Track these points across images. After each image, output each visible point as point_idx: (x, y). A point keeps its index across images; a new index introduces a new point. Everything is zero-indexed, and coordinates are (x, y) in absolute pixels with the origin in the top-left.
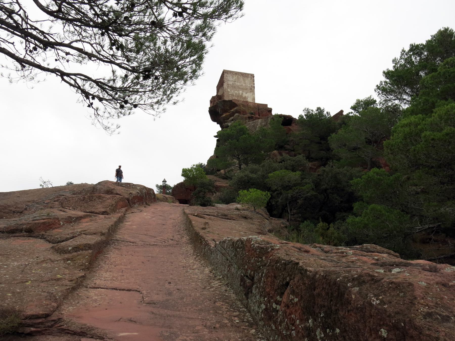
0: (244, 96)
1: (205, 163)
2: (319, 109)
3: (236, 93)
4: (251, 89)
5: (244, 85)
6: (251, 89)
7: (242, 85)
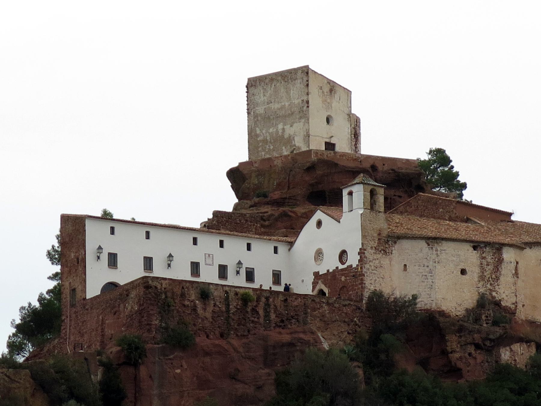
4: (301, 111)
7: (283, 107)
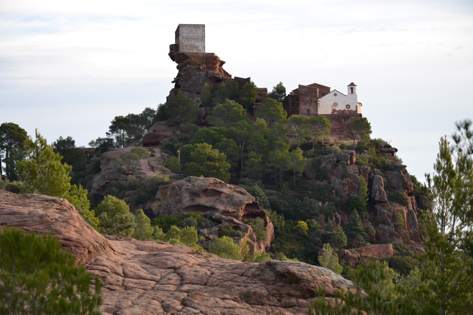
0: (196, 45)
1: (124, 117)
2: (111, 122)
3: (189, 44)
4: (202, 38)
5: (196, 35)
6: (202, 38)
7: (194, 36)
